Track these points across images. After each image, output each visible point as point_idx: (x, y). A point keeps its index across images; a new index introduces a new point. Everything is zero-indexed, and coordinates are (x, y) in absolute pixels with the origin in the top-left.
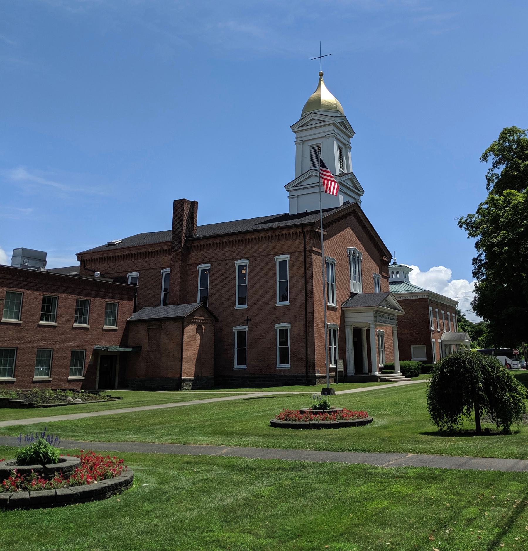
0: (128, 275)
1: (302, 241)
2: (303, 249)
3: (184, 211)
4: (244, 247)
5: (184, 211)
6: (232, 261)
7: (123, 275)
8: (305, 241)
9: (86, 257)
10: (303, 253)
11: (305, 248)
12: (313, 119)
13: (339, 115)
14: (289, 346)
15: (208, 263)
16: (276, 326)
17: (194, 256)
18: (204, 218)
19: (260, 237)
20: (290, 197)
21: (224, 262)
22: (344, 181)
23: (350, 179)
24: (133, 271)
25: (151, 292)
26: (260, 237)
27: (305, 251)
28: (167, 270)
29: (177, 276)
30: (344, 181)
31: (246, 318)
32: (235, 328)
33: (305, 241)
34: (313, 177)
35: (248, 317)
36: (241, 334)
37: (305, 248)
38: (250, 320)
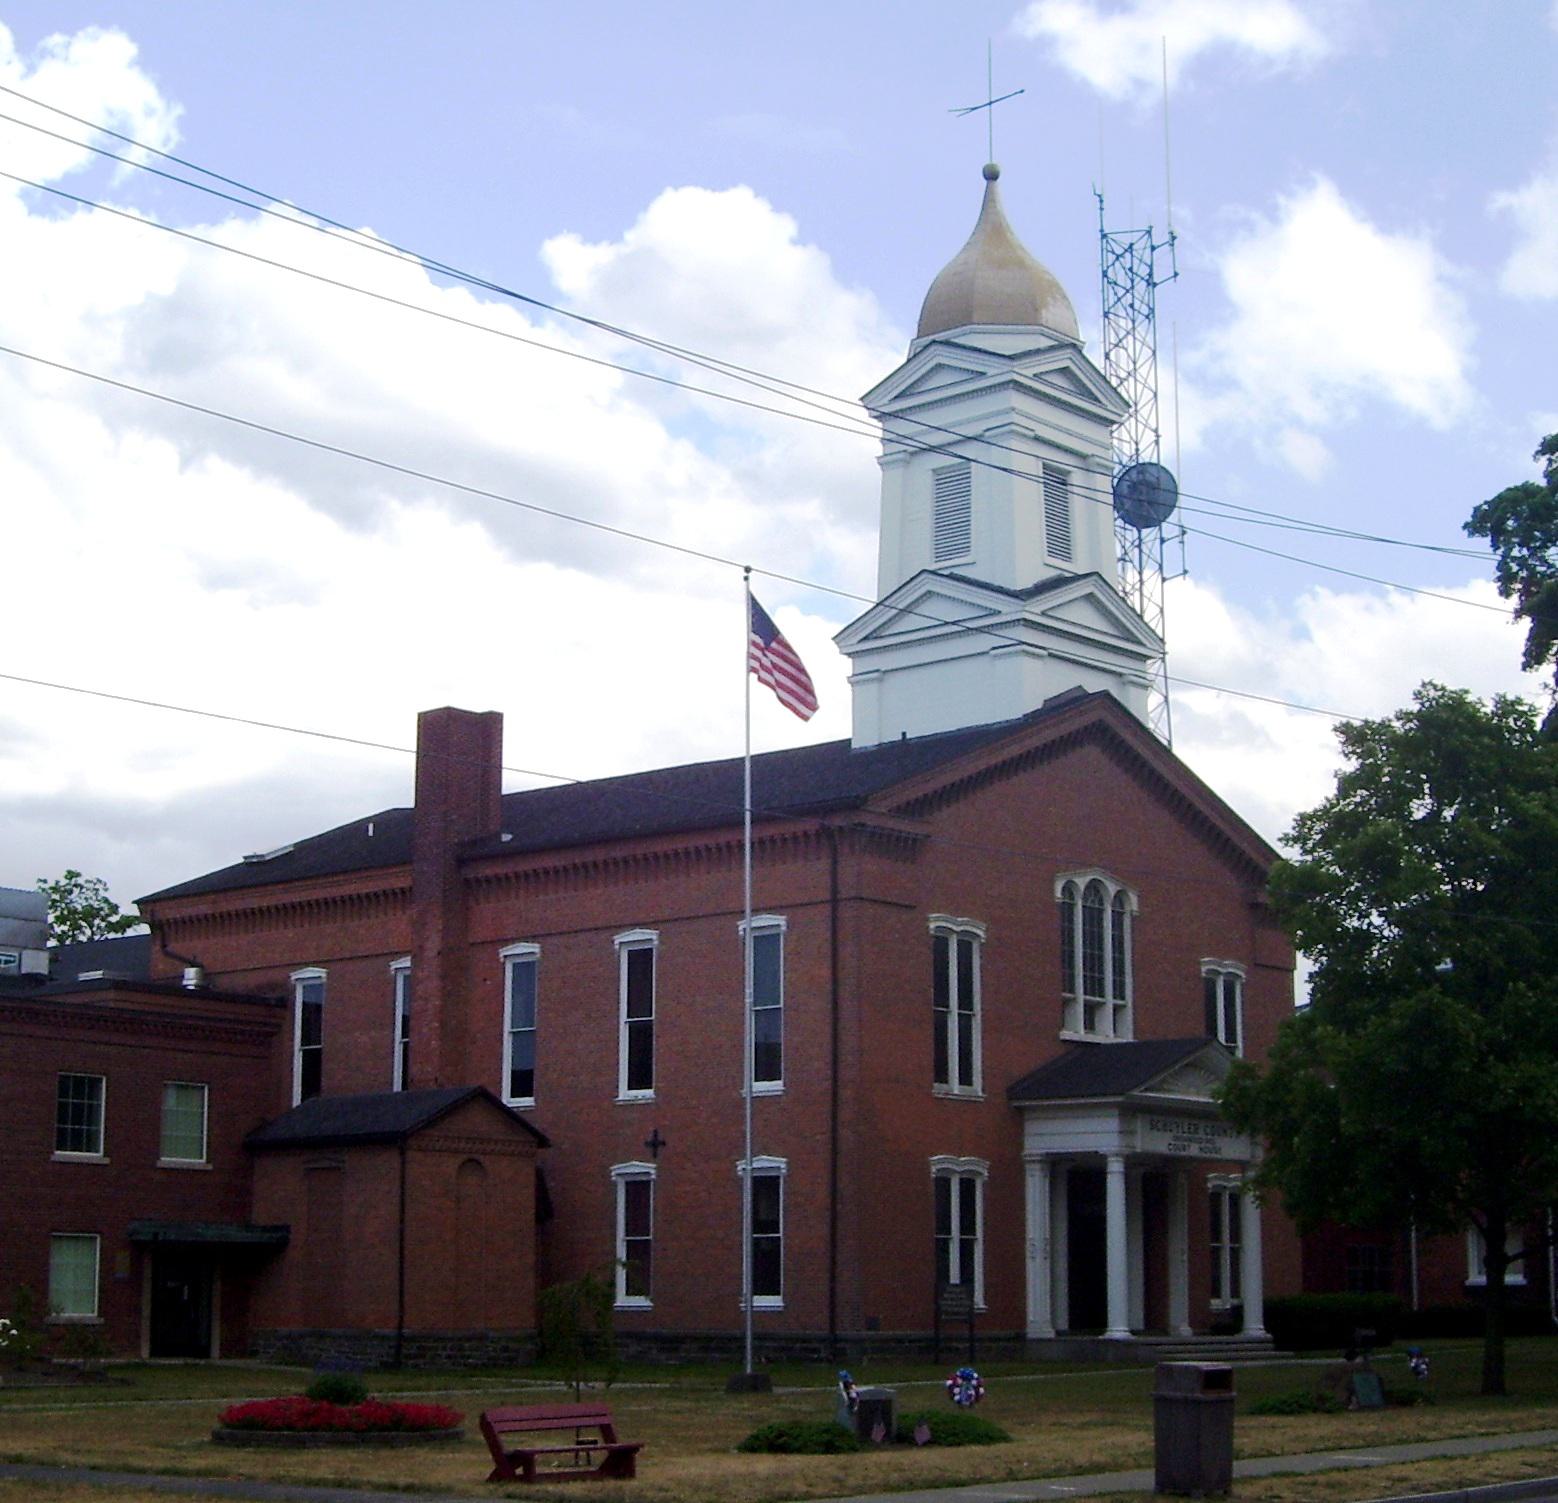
0: (294, 976)
1: (824, 864)
2: (827, 896)
3: (458, 744)
4: (1015, 780)
5: (458, 744)
6: (604, 935)
7: (275, 975)
8: (835, 862)
9: (170, 913)
10: (827, 910)
11: (835, 891)
12: (939, 367)
13: (1045, 343)
14: (781, 1235)
15: (533, 938)
16: (741, 1165)
17: (487, 912)
18: (528, 766)
19: (692, 850)
20: (855, 680)
21: (581, 936)
22: (1043, 614)
23: (1089, 597)
24: (307, 964)
25: (365, 1038)
26: (692, 850)
27: (835, 901)
28: (406, 962)
29: (431, 985)
30: (1043, 614)
31: (650, 1138)
32: (617, 1169)
33: (835, 862)
34: (934, 599)
35: (656, 1132)
36: (637, 1189)
37: (835, 891)
38: (664, 1144)
